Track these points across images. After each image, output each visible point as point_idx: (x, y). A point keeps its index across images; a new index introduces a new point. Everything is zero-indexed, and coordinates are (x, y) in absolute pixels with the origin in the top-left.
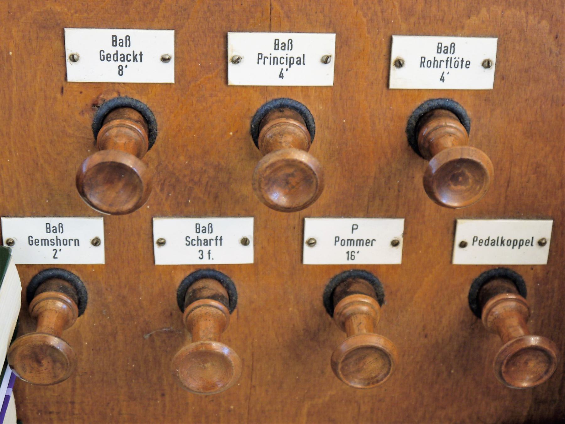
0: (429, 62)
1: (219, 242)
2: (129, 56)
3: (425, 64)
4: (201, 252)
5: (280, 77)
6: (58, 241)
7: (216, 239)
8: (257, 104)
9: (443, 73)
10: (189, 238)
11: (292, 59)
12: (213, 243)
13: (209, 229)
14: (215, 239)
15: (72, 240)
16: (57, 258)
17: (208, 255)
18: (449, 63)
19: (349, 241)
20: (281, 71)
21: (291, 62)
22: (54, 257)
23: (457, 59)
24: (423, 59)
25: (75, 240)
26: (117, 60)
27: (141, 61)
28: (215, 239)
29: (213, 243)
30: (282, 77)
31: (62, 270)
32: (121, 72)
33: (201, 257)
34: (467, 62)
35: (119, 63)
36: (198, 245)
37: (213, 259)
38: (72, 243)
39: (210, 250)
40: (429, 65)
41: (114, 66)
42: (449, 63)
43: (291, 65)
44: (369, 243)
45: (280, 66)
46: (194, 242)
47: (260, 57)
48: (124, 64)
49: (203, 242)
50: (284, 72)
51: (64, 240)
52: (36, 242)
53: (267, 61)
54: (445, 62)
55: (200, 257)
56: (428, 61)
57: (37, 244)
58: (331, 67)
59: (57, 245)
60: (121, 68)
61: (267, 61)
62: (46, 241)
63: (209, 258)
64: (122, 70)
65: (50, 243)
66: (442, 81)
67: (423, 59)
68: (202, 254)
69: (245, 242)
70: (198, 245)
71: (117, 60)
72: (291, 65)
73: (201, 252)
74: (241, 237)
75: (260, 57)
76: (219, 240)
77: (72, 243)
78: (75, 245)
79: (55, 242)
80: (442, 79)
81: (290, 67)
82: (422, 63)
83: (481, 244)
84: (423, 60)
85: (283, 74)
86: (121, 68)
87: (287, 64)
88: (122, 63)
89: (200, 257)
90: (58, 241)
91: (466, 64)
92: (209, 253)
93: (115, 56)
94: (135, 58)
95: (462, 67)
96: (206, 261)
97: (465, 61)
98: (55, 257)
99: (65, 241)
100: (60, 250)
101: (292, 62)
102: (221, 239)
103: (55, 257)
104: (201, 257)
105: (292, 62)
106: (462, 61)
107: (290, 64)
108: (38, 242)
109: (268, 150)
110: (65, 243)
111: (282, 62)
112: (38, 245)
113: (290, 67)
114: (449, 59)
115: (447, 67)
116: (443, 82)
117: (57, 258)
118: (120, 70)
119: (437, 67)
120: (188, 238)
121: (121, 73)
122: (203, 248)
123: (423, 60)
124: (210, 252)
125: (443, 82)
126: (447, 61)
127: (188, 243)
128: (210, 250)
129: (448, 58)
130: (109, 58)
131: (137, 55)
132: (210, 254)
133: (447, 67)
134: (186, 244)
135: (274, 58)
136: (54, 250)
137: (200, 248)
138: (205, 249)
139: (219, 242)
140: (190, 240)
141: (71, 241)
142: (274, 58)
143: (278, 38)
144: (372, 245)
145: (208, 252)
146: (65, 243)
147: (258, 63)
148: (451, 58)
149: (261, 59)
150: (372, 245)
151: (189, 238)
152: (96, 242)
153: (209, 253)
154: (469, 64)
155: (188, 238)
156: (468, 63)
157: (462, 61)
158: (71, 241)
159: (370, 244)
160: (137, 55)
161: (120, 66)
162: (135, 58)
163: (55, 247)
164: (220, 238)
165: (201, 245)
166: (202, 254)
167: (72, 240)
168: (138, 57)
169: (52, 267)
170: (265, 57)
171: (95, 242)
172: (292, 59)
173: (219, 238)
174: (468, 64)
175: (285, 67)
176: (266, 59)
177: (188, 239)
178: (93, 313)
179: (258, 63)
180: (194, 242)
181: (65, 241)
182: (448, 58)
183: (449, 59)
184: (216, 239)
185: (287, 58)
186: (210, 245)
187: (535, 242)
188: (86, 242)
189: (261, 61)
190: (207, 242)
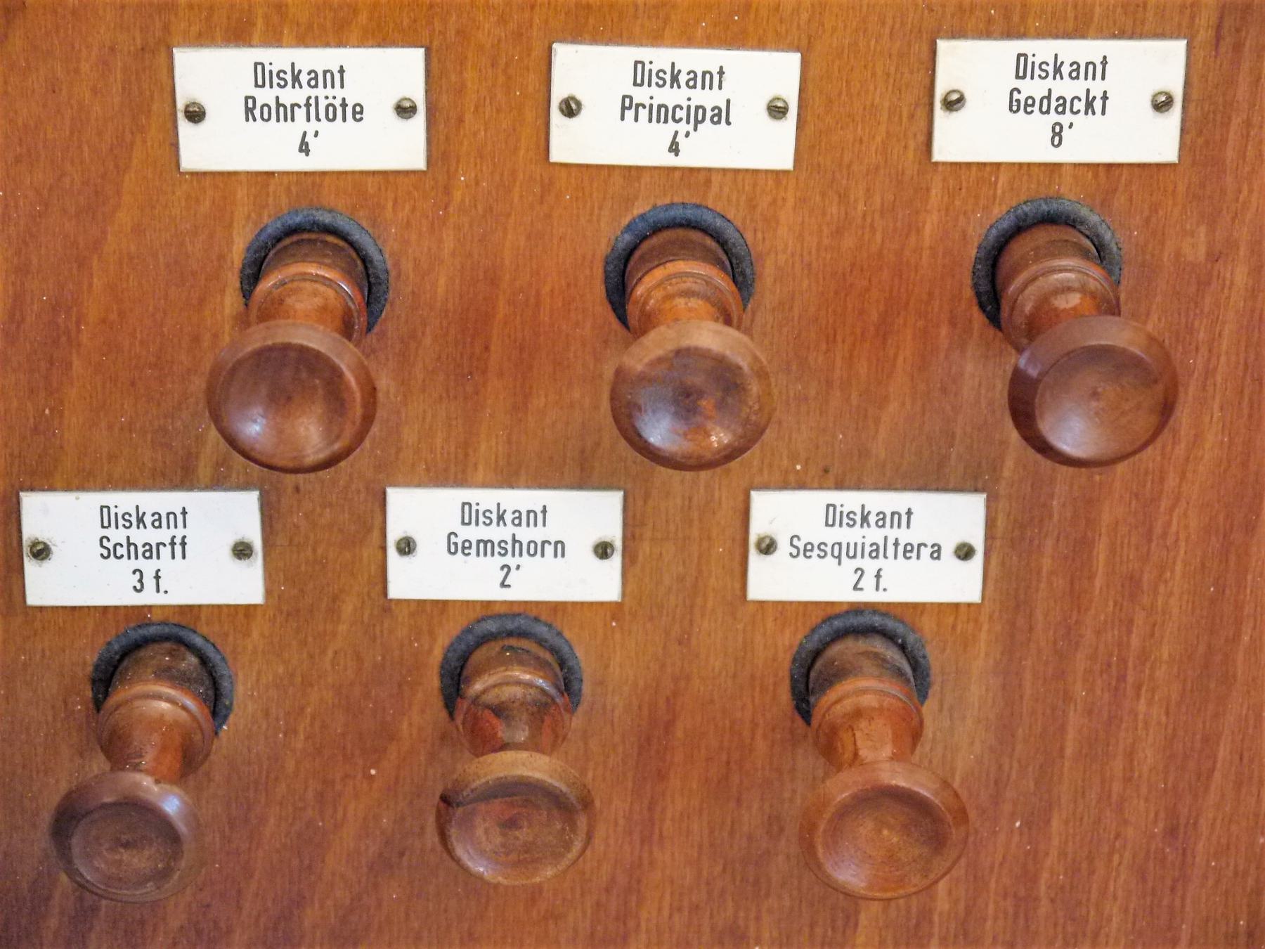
0: (266, 109)
1: (178, 549)
2: (678, 109)
3: (257, 112)
4: (138, 573)
5: (301, 150)
6: (517, 545)
7: (173, 544)
8: (999, 213)
9: (305, 134)
10: (109, 540)
11: (700, 111)
12: (166, 552)
13: (537, 517)
14: (170, 544)
15: (549, 543)
16: (509, 586)
17: (154, 581)
18: (312, 109)
19: (482, 545)
20: (675, 137)
21: (697, 116)
22: (503, 585)
23: (330, 101)
24: (250, 102)
25: (557, 543)
26: (1048, 112)
27: (1103, 113)
28: (170, 544)
29: (166, 552)
30: (307, 152)
31: (885, 615)
32: (1057, 139)
33: (139, 587)
34: (354, 107)
35: (1053, 117)
36: (129, 558)
37: (166, 592)
38: (549, 549)
39: (880, 570)
40: (266, 116)
41: (1041, 124)
42: (312, 109)
43: (699, 125)
44: (911, 551)
45: (672, 126)
46: (120, 551)
47: (627, 104)
48: (1065, 119)
49: (141, 550)
50: (309, 139)
51: (529, 543)
52: (807, 550)
53: (643, 113)
54: (304, 109)
55: (135, 587)
56: (262, 107)
57: (466, 551)
58: (1173, 119)
59: (513, 555)
60: (1057, 129)
61: (643, 113)
62: (489, 545)
63: (158, 591)
64: (1059, 134)
65: (497, 549)
66: (304, 154)
67: (250, 102)
68: (140, 581)
69: (242, 551)
70: (129, 558)
71: (1048, 112)
72: (699, 125)
73: (138, 573)
74: (231, 540)
75: (627, 104)
76: (180, 546)
77: (549, 549)
78: (556, 555)
79: (509, 547)
80: (304, 148)
81: (695, 129)
82: (249, 111)
83: (908, 555)
84: (250, 105)
85: (307, 144)
86: (1057, 129)
87: (688, 122)
88: (1060, 119)
89: (135, 587)
90: (517, 545)
91: (354, 113)
92: (157, 577)
93: (1045, 102)
94: (1089, 105)
95: (344, 120)
96: (869, 595)
97: (350, 103)
98: (506, 583)
99: (532, 545)
100: (518, 567)
101: (700, 118)
102: (183, 544)
103: (506, 583)
104: (139, 587)
105: (700, 118)
106: (344, 105)
107: (697, 122)
108: (470, 547)
109: (648, 322)
110: (532, 551)
111: (1075, 110)
112: (469, 554)
113: (695, 129)
114: (312, 101)
115: (308, 120)
116: (307, 155)
117: (509, 586)
118: (1055, 134)
119: (286, 120)
120: (795, 539)
121: (1056, 142)
122: (141, 563)
123: (250, 105)
124: (881, 573)
125: (307, 155)
126: (308, 105)
127: (794, 552)
128: (880, 570)
129: (310, 97)
130: (358, 113)
131: (1094, 98)
132: (881, 579)
133: (308, 120)
134: (102, 555)
135: (660, 107)
136: (134, 572)
137: (134, 564)
138: (149, 567)
139: (178, 549)
140: (110, 545)
141: (546, 545)
142: (660, 107)
143: (642, 60)
144: (918, 557)
145: (154, 575)
146: (532, 551)
147: (622, 118)
148: (317, 98)
149: (630, 108)
150: (918, 557)
151: (799, 539)
152: (406, 547)
153: (157, 577)
154: (361, 112)
155: (795, 539)
156: (358, 109)
157: (344, 105)
158: (922, 547)
159: (914, 554)
160: (1094, 98)
161: (1057, 124)
162: (1089, 105)
163: (508, 560)
164: (180, 541)
165: (136, 558)
166: (140, 581)
167: (549, 543)
168: (1098, 105)
169: (516, 610)
170: (638, 106)
171: (764, 545)
172: (700, 111)
173: (178, 540)
174: (358, 113)
175: (683, 127)
176: (640, 108)
177: (795, 541)
178: (487, 724)
179: (622, 118)
180: (120, 551)
181: (532, 545)
182: (310, 97)
183: (312, 101)
184: (173, 544)
185: (689, 107)
186: (158, 557)
187: (784, 547)
188: (580, 550)
189: (630, 114)
190: (151, 551)
